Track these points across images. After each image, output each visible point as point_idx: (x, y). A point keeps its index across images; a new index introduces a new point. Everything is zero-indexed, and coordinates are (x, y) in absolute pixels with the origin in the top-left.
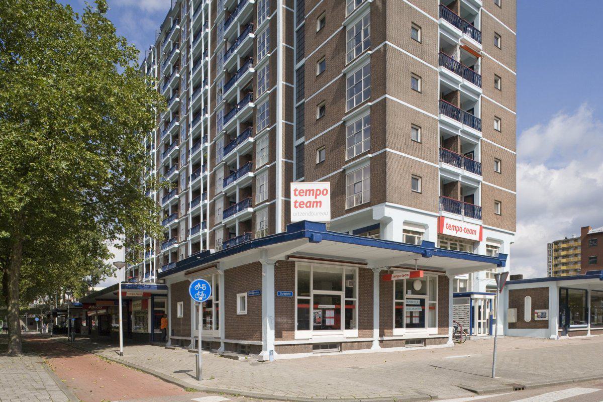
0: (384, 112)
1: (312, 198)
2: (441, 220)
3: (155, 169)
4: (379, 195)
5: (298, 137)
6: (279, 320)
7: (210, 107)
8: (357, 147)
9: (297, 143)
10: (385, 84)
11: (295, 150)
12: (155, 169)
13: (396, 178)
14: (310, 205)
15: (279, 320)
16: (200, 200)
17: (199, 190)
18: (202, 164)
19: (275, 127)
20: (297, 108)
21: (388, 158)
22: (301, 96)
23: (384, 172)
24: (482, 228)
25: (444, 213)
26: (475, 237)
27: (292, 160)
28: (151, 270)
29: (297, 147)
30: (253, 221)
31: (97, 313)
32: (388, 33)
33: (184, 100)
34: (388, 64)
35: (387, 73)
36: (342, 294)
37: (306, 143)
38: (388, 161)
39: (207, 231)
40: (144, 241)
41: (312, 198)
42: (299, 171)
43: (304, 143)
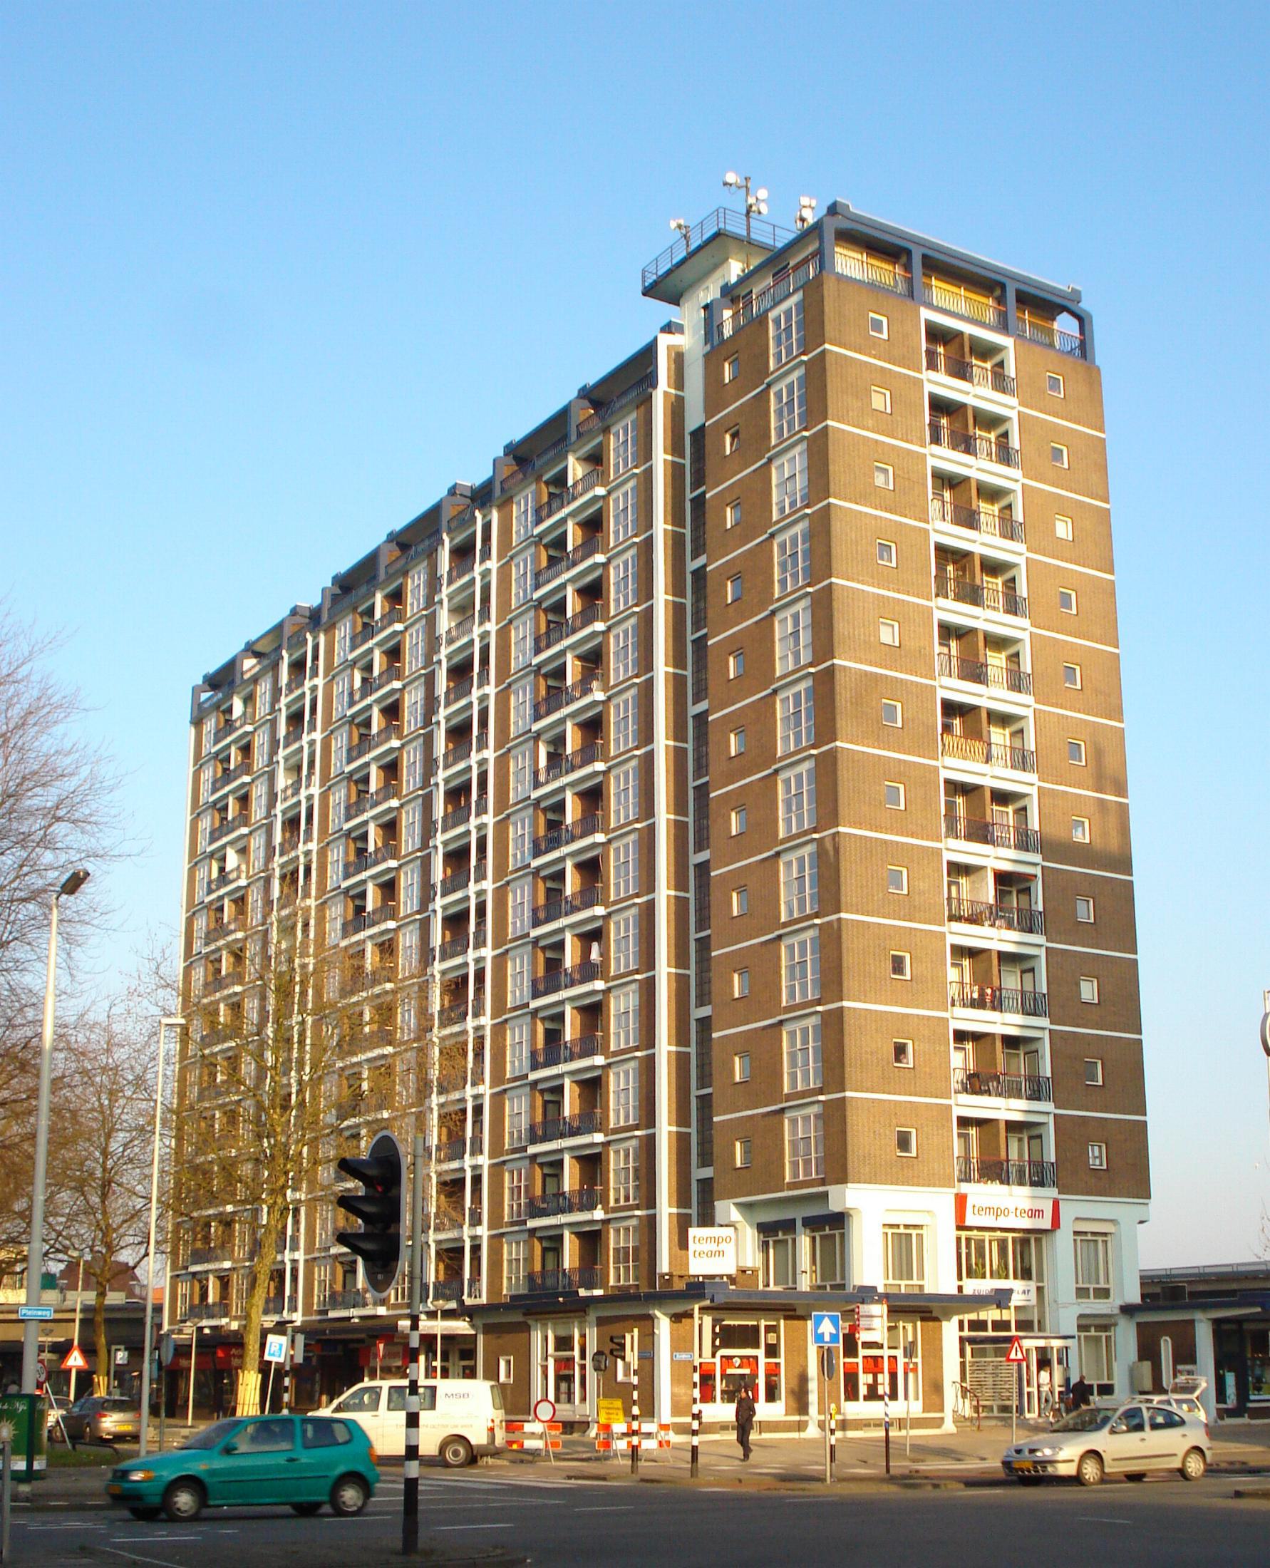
0: (824, 369)
1: (713, 1247)
2: (961, 1201)
3: (313, 893)
4: (837, 1168)
5: (695, 556)
6: (676, 1390)
7: (499, 536)
8: (789, 423)
9: (694, 710)
10: (840, 984)
11: (692, 870)
12: (313, 893)
13: (864, 1137)
14: (712, 1254)
15: (676, 1390)
16: (472, 686)
17: (466, 787)
18: (478, 607)
19: (651, 466)
20: (692, 500)
21: (849, 1108)
22: (699, 480)
23: (844, 1132)
24: (1056, 1204)
25: (965, 1188)
26: (1046, 1223)
27: (687, 891)
28: (287, 1293)
29: (693, 573)
30: (604, 650)
31: (30, 1465)
32: (843, 899)
33: (419, 574)
34: (844, 951)
35: (845, 965)
36: (760, 1352)
37: (708, 496)
38: (848, 1113)
39: (488, 952)
40: (275, 865)
41: (713, 1247)
42: (702, 990)
43: (705, 566)
